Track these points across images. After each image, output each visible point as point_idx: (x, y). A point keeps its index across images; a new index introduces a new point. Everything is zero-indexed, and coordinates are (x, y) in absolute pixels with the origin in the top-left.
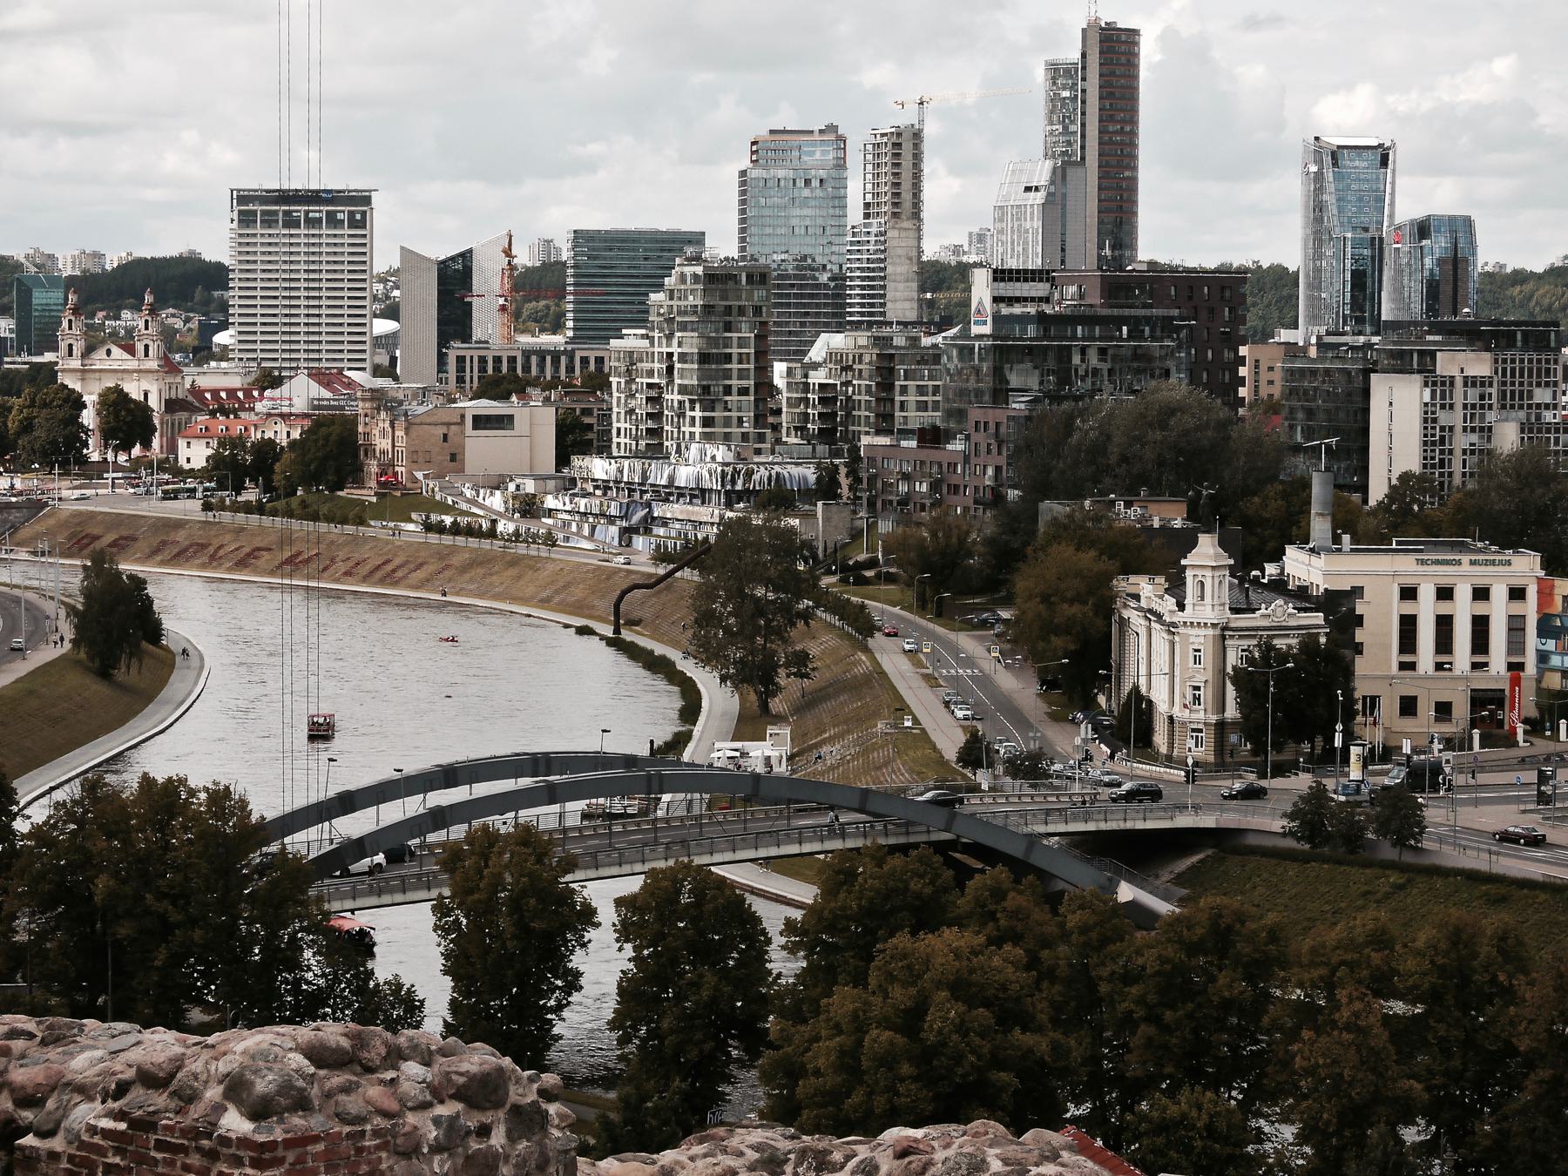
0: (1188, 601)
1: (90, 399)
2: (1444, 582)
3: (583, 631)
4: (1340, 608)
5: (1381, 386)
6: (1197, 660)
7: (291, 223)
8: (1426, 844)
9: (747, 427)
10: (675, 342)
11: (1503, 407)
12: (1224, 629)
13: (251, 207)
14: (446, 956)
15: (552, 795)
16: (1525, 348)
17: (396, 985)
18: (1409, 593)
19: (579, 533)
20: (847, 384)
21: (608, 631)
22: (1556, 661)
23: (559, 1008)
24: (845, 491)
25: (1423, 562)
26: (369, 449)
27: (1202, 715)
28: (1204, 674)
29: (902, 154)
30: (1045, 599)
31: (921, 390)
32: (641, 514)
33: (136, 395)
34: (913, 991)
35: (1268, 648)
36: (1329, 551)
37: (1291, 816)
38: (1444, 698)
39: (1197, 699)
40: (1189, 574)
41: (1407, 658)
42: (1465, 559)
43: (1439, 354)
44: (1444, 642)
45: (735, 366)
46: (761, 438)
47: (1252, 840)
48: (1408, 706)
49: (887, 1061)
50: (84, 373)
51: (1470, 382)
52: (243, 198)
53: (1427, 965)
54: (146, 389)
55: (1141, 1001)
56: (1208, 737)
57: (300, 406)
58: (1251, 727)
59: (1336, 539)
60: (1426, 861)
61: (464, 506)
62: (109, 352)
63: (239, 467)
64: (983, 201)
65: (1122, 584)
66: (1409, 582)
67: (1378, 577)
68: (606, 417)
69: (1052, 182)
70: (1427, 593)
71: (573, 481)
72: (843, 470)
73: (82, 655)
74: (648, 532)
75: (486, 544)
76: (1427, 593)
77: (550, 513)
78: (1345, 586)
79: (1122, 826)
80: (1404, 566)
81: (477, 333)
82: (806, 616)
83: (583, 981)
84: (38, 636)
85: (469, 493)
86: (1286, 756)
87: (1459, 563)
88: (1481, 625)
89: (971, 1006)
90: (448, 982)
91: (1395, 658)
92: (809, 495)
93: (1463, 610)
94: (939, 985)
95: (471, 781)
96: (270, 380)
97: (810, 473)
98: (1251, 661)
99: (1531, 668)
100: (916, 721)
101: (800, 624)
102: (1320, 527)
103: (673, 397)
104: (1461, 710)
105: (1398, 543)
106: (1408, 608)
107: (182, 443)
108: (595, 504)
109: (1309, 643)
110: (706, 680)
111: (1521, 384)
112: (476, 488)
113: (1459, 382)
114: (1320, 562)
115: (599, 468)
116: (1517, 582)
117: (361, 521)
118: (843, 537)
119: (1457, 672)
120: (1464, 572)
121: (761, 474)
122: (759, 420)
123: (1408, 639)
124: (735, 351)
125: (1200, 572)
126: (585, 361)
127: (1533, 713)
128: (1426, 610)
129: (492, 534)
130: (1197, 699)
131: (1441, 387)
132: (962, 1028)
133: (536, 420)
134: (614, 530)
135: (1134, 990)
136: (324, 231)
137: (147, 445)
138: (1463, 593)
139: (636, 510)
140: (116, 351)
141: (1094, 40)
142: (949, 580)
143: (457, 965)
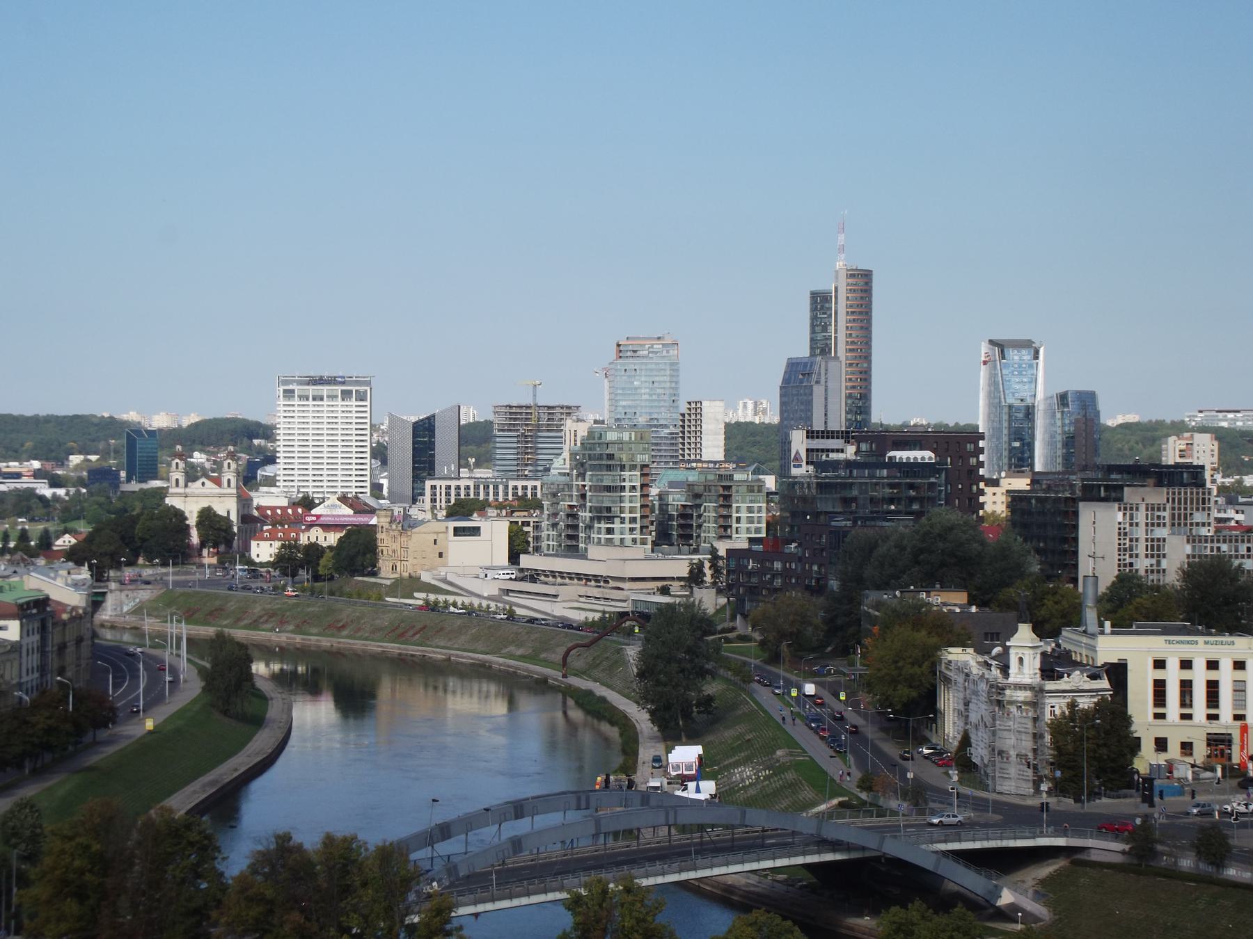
2: (1186, 657)
10: (587, 478)
11: (1173, 525)
13: (291, 387)
18: (1160, 664)
25: (1170, 642)
31: (750, 510)
33: (222, 512)
35: (1072, 705)
40: (1012, 651)
42: (1201, 639)
43: (1126, 489)
45: (627, 494)
54: (227, 507)
62: (203, 484)
66: (1160, 656)
67: (1137, 650)
70: (1173, 664)
72: (707, 565)
76: (1173, 664)
80: (1172, 648)
87: (1196, 642)
88: (1213, 687)
91: (1151, 710)
93: (1199, 677)
103: (585, 515)
104: (1201, 752)
105: (1138, 627)
106: (1160, 674)
109: (1101, 707)
111: (1185, 509)
125: (1020, 651)
126: (515, 488)
128: (1173, 676)
141: (843, 275)
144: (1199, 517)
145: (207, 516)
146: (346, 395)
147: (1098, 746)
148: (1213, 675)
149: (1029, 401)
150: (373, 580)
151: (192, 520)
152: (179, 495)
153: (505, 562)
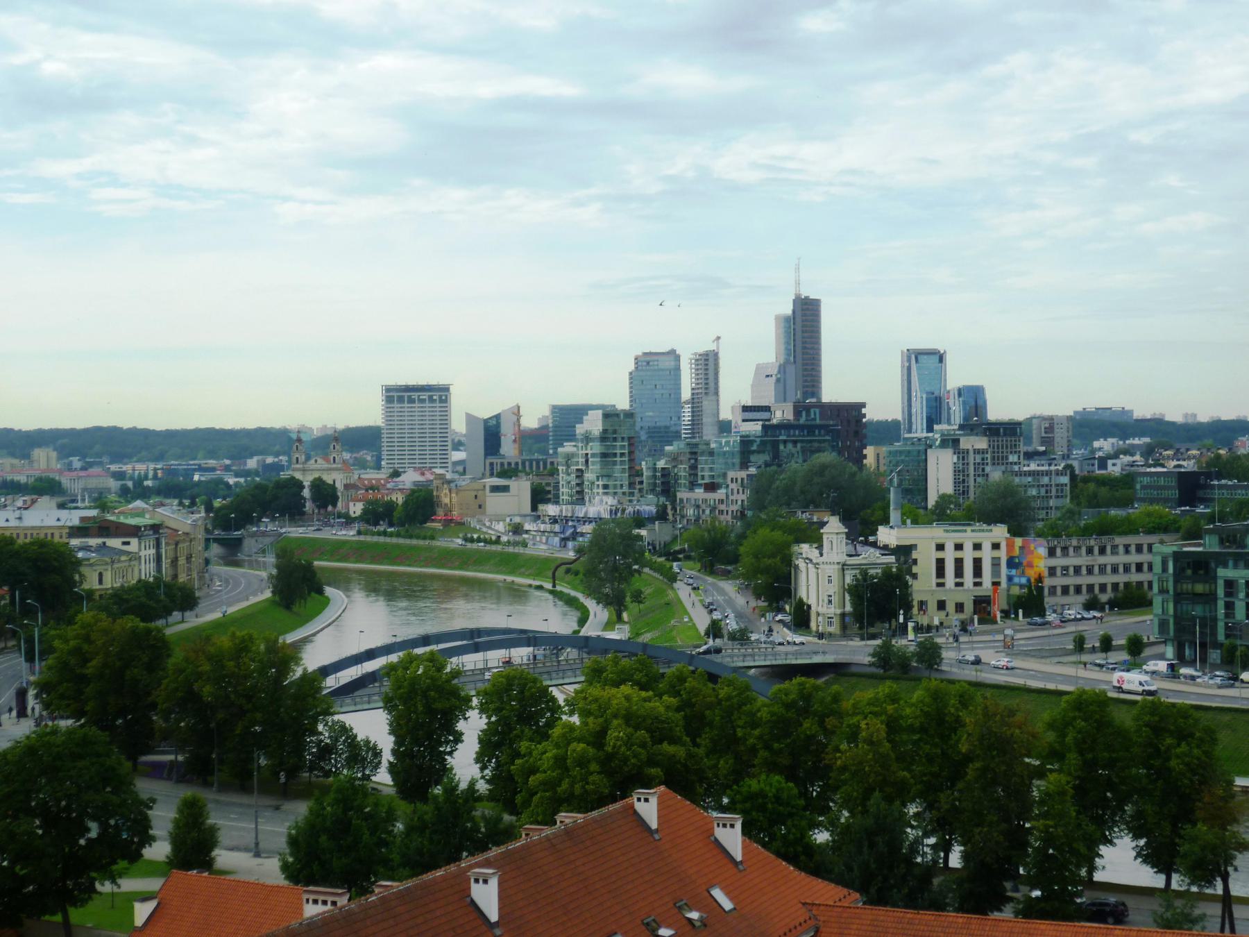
0: (825, 551)
1: (306, 484)
2: (959, 541)
3: (540, 588)
4: (904, 552)
5: (932, 455)
6: (830, 582)
7: (411, 401)
8: (944, 668)
9: (625, 489)
12: (844, 565)
14: (391, 725)
15: (477, 648)
16: (1005, 435)
17: (367, 742)
18: (940, 547)
19: (541, 541)
20: (675, 467)
21: (549, 586)
22: (1016, 580)
23: (450, 753)
24: (670, 517)
25: (947, 531)
26: (439, 504)
27: (834, 610)
28: (834, 589)
29: (708, 364)
30: (756, 557)
32: (571, 530)
34: (601, 720)
35: (864, 573)
36: (899, 527)
37: (873, 655)
38: (960, 601)
39: (830, 602)
40: (825, 537)
41: (941, 581)
42: (969, 529)
44: (959, 572)
45: (618, 459)
46: (632, 494)
47: (854, 669)
48: (941, 605)
49: (582, 762)
50: (304, 470)
51: (977, 452)
52: (389, 389)
53: (918, 713)
55: (760, 738)
56: (836, 621)
57: (408, 485)
58: (858, 616)
59: (904, 523)
60: (944, 676)
61: (484, 530)
63: (378, 514)
64: (746, 381)
65: (795, 548)
66: (940, 541)
67: (925, 540)
68: (557, 487)
69: (779, 372)
70: (949, 547)
71: (539, 517)
73: (277, 598)
74: (574, 539)
75: (494, 548)
76: (949, 547)
77: (527, 532)
78: (908, 543)
79: (784, 662)
80: (937, 532)
81: (502, 451)
82: (639, 572)
83: (464, 738)
85: (488, 524)
86: (872, 630)
88: (977, 563)
89: (637, 728)
90: (392, 738)
91: (934, 580)
92: (652, 520)
93: (968, 555)
94: (615, 716)
95: (437, 643)
96: (396, 474)
97: (653, 509)
98: (857, 580)
99: (1004, 584)
100: (691, 620)
101: (636, 575)
102: (894, 516)
104: (969, 607)
106: (940, 555)
107: (351, 504)
108: (548, 527)
109: (887, 574)
110: (591, 604)
112: (491, 521)
113: (971, 453)
114: (894, 532)
115: (551, 510)
116: (996, 541)
117: (432, 538)
118: (668, 538)
119: (966, 586)
120: (969, 536)
121: (630, 510)
122: (631, 485)
123: (940, 571)
124: (618, 452)
127: (1005, 607)
128: (950, 556)
129: (498, 541)
130: (830, 602)
131: (962, 455)
132: (628, 743)
133: (521, 488)
134: (557, 540)
135: (757, 732)
136: (406, 405)
137: (335, 505)
138: (968, 547)
139: (566, 528)
140: (320, 461)
142: (715, 553)
143: (395, 729)
145: (318, 485)
149: (937, 393)
152: (298, 470)
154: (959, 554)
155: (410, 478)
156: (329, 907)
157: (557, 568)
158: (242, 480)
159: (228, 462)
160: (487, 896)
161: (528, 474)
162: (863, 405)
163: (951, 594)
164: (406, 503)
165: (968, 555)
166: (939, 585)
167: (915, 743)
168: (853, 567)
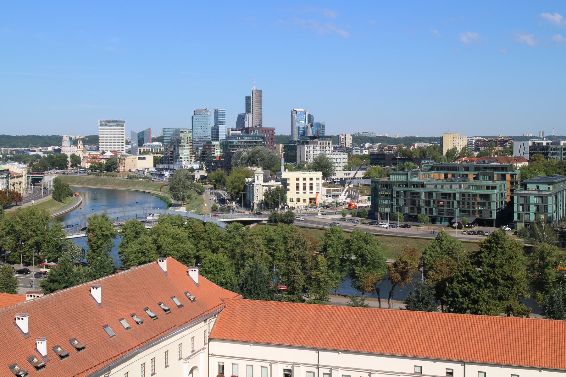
18: (298, 179)
35: (270, 188)
42: (308, 173)
44: (304, 189)
66: (298, 177)
70: (301, 179)
76: (301, 179)
84: (45, 195)
88: (311, 185)
91: (296, 191)
93: (308, 182)
104: (308, 201)
106: (298, 182)
109: (278, 188)
128: (301, 182)
137: (80, 163)
144: (327, 148)
145: (73, 156)
146: (118, 125)
147: (479, 286)
148: (311, 182)
150: (283, 168)
151: (69, 155)
153: (153, 166)
154: (304, 182)
155: (108, 154)
156: (33, 298)
157: (161, 187)
158: (46, 155)
159: (40, 148)
160: (97, 294)
161: (152, 153)
162: (274, 129)
163: (302, 196)
164: (106, 163)
165: (308, 182)
166: (297, 193)
167: (317, 254)
168: (266, 186)
